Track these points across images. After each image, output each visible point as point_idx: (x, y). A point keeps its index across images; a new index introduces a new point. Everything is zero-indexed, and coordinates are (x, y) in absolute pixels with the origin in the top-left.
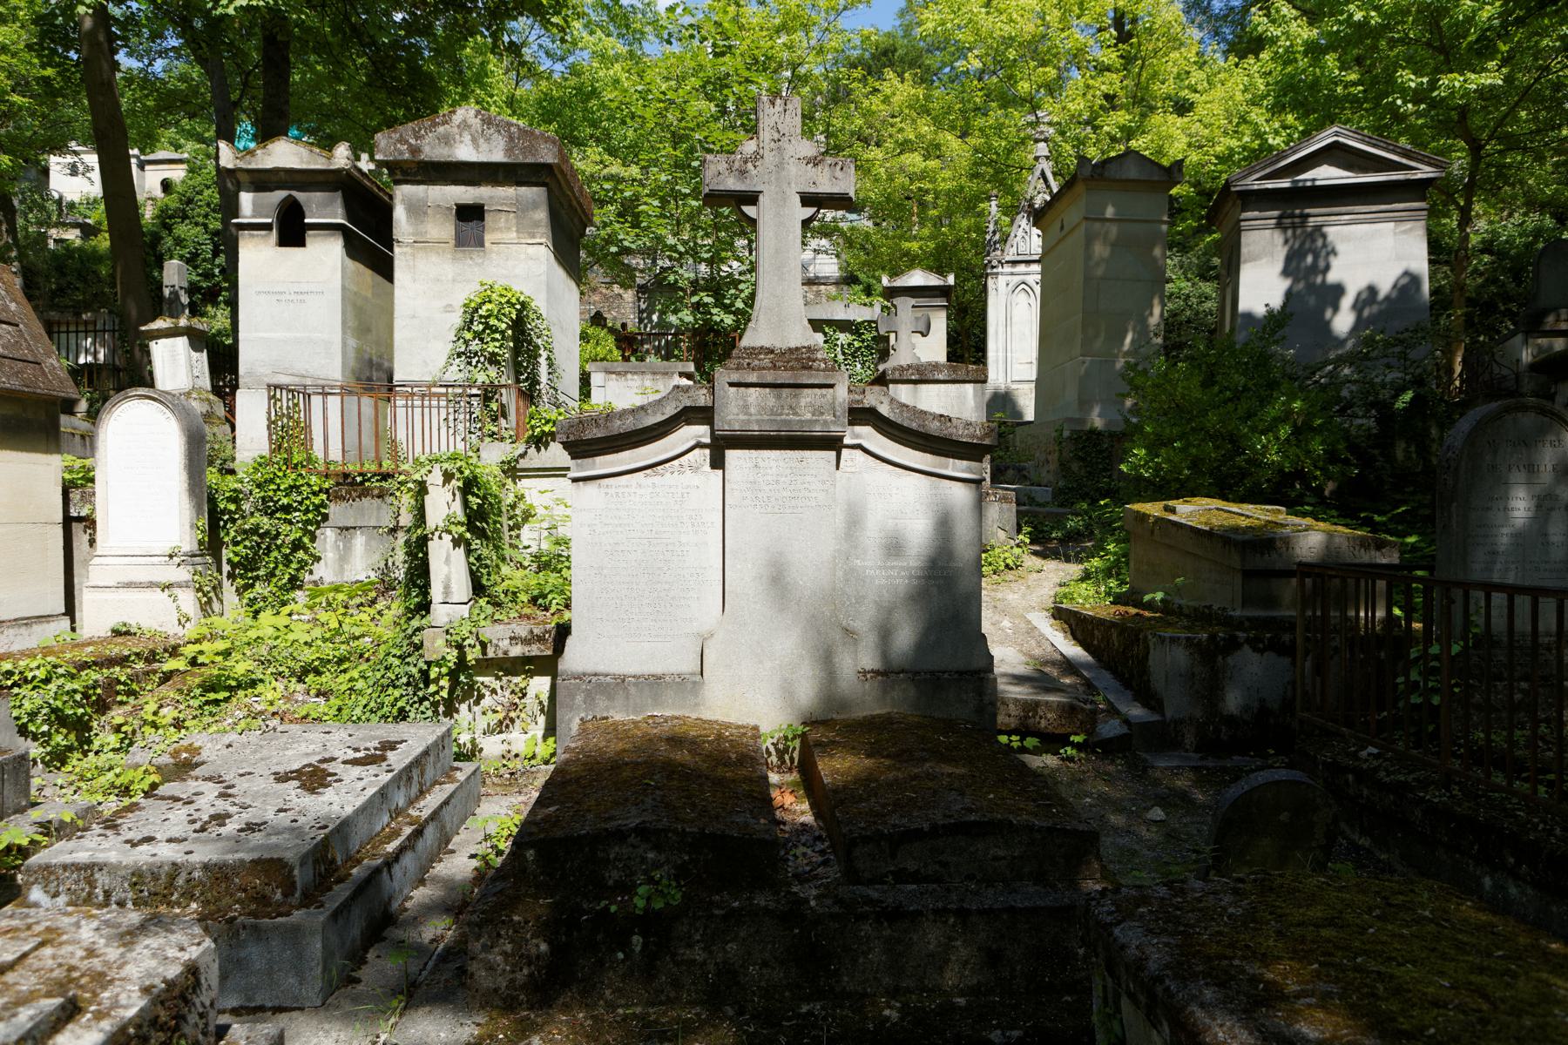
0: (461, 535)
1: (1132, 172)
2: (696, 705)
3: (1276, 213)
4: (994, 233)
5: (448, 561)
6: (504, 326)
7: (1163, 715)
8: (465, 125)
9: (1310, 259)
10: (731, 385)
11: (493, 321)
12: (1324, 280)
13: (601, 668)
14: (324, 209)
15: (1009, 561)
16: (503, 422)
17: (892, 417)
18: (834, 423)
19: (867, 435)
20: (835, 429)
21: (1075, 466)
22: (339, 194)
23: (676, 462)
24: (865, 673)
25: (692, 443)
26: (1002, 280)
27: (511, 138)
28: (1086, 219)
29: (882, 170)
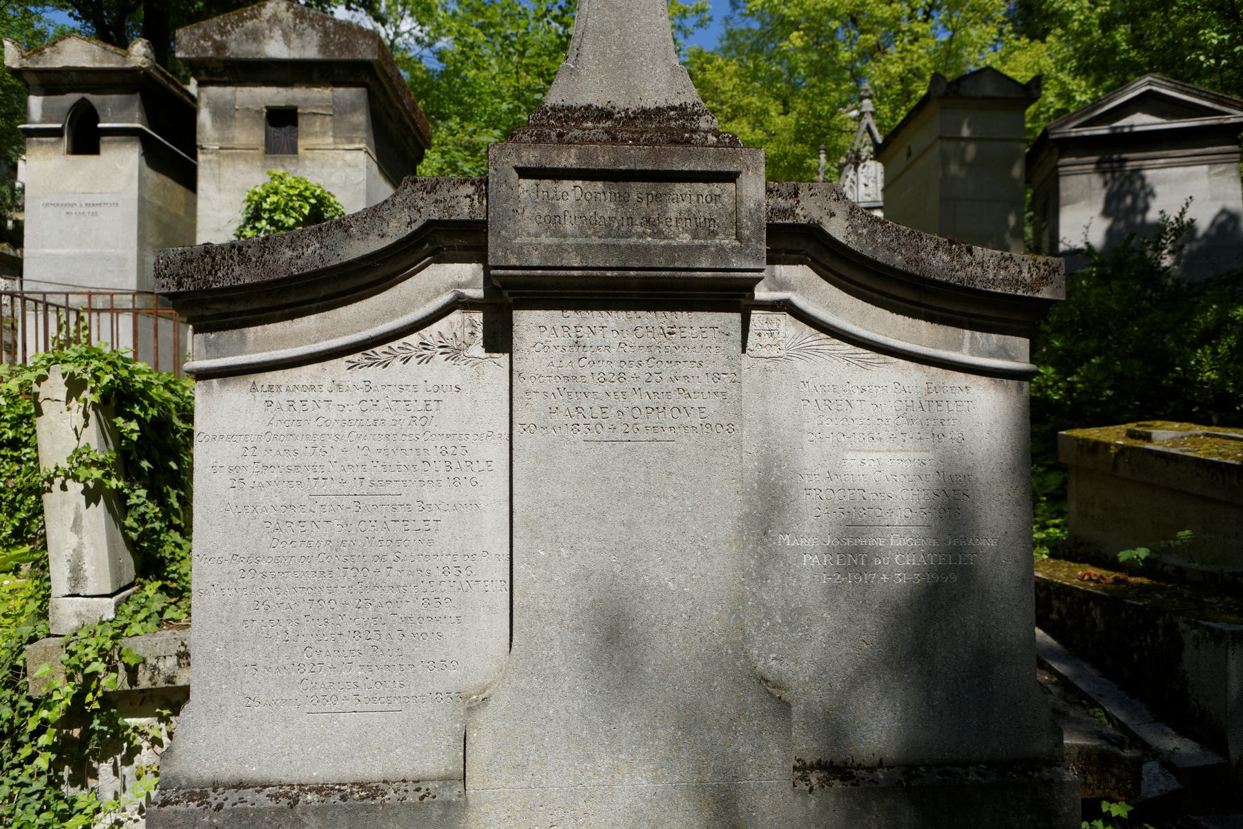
1: (988, 89)
3: (1094, 158)
5: (77, 526)
7: (1225, 753)
8: (275, 20)
9: (1129, 200)
10: (524, 173)
12: (1143, 220)
13: (252, 771)
14: (121, 113)
18: (739, 252)
19: (801, 282)
22: (138, 96)
23: (413, 339)
24: (803, 769)
25: (446, 298)
27: (326, 33)
28: (941, 138)
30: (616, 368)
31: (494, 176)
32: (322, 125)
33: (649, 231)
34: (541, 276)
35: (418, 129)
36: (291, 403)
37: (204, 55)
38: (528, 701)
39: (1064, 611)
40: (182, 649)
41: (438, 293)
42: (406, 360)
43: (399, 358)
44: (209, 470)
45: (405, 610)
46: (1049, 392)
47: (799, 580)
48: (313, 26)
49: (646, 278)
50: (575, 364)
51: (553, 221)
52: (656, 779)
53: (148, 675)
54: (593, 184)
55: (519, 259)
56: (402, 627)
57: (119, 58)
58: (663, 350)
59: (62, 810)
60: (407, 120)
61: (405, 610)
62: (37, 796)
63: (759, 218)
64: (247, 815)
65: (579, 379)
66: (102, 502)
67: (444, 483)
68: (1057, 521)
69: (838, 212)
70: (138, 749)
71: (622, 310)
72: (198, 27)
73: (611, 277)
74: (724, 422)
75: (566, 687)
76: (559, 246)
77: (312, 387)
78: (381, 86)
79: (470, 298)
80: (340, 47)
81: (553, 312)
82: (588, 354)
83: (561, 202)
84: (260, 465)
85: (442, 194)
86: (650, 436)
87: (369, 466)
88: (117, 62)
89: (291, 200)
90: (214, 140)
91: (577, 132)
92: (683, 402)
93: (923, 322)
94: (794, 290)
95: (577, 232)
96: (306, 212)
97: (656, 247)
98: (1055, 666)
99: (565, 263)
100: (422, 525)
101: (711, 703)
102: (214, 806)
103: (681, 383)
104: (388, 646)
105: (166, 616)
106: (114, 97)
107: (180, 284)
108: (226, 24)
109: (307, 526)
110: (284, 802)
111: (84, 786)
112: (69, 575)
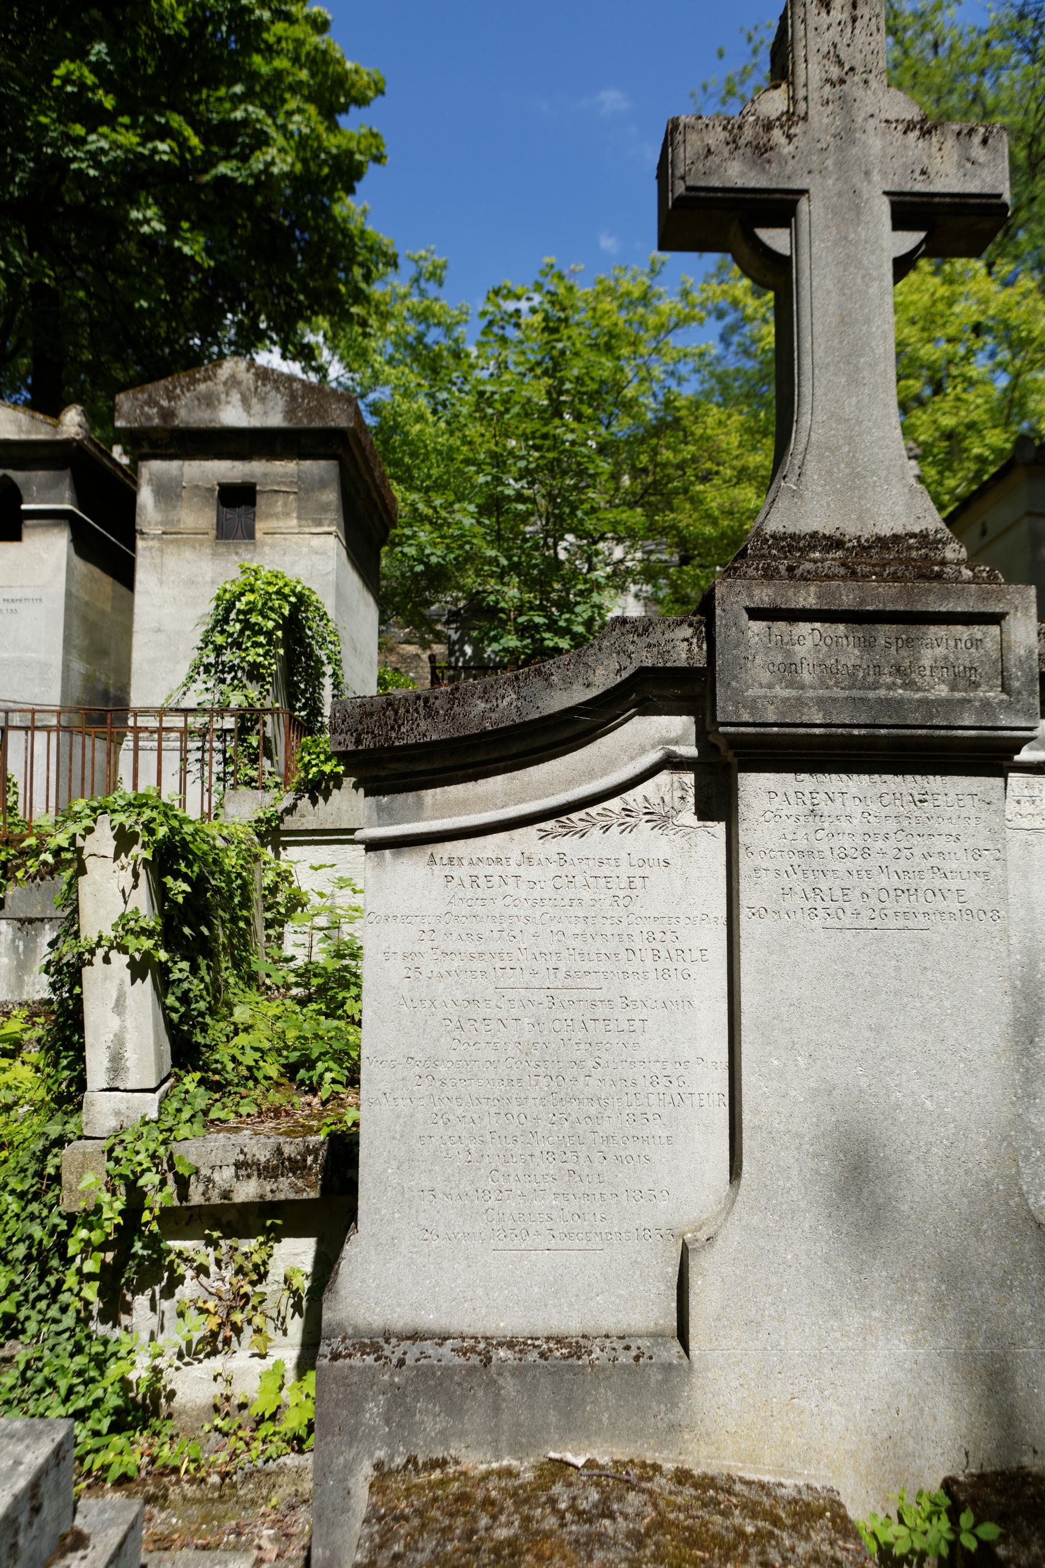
0: (147, 955)
2: (674, 1428)
5: (119, 1006)
6: (271, 624)
8: (233, 382)
10: (755, 614)
11: (254, 618)
13: (430, 1319)
16: (266, 763)
18: (1008, 707)
23: (615, 804)
27: (293, 397)
28: (1030, 514)
30: (859, 841)
32: (285, 504)
33: (899, 681)
35: (385, 506)
36: (474, 878)
37: (147, 424)
38: (762, 1242)
40: (241, 1157)
41: (643, 750)
42: (606, 829)
44: (381, 957)
45: (606, 1127)
48: (277, 389)
49: (898, 737)
50: (811, 837)
51: (789, 670)
52: (917, 1343)
53: (201, 1188)
54: (834, 626)
55: (752, 714)
57: (49, 428)
58: (913, 821)
59: (97, 1354)
60: (375, 495)
61: (606, 1127)
62: (67, 1335)
63: (1031, 668)
64: (434, 1374)
65: (816, 854)
66: (149, 978)
67: (652, 975)
70: (181, 1279)
71: (865, 773)
72: (142, 392)
73: (859, 736)
74: (987, 908)
75: (806, 1226)
76: (799, 699)
77: (499, 860)
79: (681, 756)
80: (309, 413)
83: (797, 647)
84: (439, 952)
86: (901, 923)
87: (565, 954)
88: (47, 433)
89: (271, 600)
90: (156, 524)
92: (938, 882)
96: (286, 613)
97: (910, 701)
99: (805, 719)
100: (625, 1025)
101: (981, 1250)
102: (395, 1361)
103: (935, 861)
104: (587, 1171)
105: (213, 1115)
106: (41, 473)
107: (358, 742)
108: (175, 388)
109: (494, 1025)
110: (475, 1360)
111: (116, 1323)
112: (109, 1065)
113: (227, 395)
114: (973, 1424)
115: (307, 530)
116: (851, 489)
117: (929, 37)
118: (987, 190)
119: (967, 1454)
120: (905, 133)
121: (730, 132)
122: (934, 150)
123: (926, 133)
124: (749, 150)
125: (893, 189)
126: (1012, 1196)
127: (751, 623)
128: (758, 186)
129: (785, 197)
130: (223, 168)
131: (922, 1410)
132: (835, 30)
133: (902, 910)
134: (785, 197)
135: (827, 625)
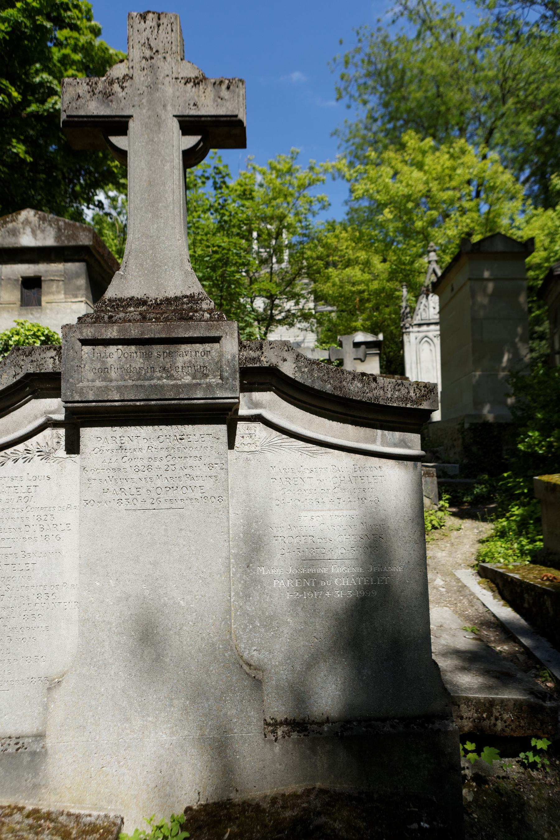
1: (500, 247)
2: (36, 786)
4: (406, 308)
8: (27, 222)
10: (85, 342)
15: (435, 523)
17: (299, 378)
18: (221, 387)
19: (269, 403)
20: (223, 395)
21: (474, 449)
23: (20, 447)
24: (274, 725)
25: (41, 421)
26: (412, 336)
27: (59, 229)
28: (470, 279)
29: (337, 279)
30: (146, 462)
31: (65, 345)
32: (57, 287)
33: (164, 375)
34: (95, 407)
38: (87, 683)
39: (531, 602)
41: (36, 418)
42: (16, 461)
43: (11, 459)
46: (537, 448)
47: (271, 597)
48: (51, 225)
49: (162, 405)
50: (120, 461)
51: (104, 371)
52: (172, 734)
54: (129, 347)
55: (80, 396)
56: (10, 634)
63: (234, 365)
65: (122, 470)
68: (541, 537)
69: (288, 359)
71: (150, 425)
73: (140, 406)
74: (215, 495)
75: (112, 674)
76: (106, 387)
78: (97, 260)
79: (56, 421)
80: (68, 237)
81: (105, 428)
82: (128, 454)
83: (109, 359)
85: (35, 357)
86: (168, 505)
91: (122, 315)
92: (189, 483)
93: (350, 426)
94: (265, 408)
95: (119, 378)
97: (168, 385)
98: (523, 640)
99: (110, 398)
100: (24, 567)
101: (209, 681)
113: (24, 229)
114: (202, 777)
115: (69, 300)
116: (153, 273)
117: (449, 32)
118: (229, 113)
119: (199, 793)
120: (185, 84)
121: (91, 86)
122: (201, 93)
123: (196, 84)
124: (100, 95)
125: (178, 114)
126: (227, 651)
127: (84, 347)
128: (105, 114)
129: (121, 119)
130: (33, 107)
131: (174, 770)
132: (148, 31)
133: (169, 498)
134: (121, 119)
135: (125, 347)
